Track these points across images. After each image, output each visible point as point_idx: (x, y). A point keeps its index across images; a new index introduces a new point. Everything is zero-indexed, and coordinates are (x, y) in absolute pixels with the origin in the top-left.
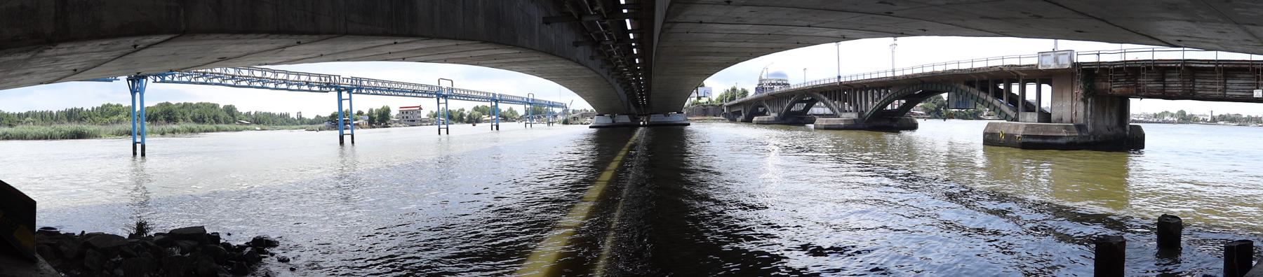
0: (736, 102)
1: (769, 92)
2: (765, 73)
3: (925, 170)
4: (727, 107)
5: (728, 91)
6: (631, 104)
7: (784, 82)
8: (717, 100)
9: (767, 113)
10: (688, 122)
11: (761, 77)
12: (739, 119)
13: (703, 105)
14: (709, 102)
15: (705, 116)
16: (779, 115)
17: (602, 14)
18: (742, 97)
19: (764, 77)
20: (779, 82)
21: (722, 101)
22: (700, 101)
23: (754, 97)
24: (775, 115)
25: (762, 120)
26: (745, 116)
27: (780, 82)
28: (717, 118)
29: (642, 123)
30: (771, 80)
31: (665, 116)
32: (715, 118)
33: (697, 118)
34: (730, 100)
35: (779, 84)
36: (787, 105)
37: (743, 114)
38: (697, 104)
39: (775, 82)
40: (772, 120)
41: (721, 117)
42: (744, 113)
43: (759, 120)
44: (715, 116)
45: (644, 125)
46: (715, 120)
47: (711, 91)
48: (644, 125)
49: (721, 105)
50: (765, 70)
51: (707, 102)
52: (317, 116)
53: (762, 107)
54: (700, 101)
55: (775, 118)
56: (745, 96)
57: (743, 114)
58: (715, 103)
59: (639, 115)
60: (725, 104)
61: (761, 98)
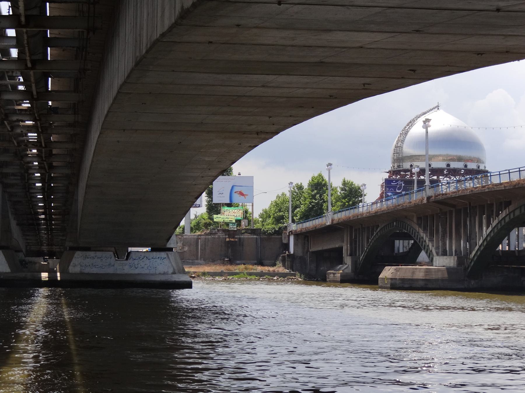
0: (327, 220)
1: (430, 192)
2: (417, 130)
3: (514, 356)
4: (298, 235)
5: (300, 188)
6: (11, 217)
7: (472, 166)
8: (266, 215)
9: (423, 256)
10: (184, 278)
11: (398, 149)
12: (337, 273)
13: (225, 226)
14: (244, 223)
15: (231, 262)
16: (461, 260)
17: (32, 93)
18: (344, 208)
19: (407, 150)
20: (454, 165)
21: (279, 220)
22: (217, 218)
23: (375, 208)
24: (450, 261)
25: (408, 276)
26: (355, 263)
27: (459, 165)
28: (266, 269)
29: (45, 275)
30: (431, 158)
31: (117, 255)
32: (259, 269)
33: (207, 269)
34: (306, 216)
35: (454, 172)
36: (486, 231)
37: (348, 260)
38: (207, 225)
39: (442, 165)
40: (439, 276)
41: (280, 268)
42: (352, 254)
43: (399, 276)
44: (261, 263)
45: (51, 283)
46: (261, 275)
47: (251, 188)
48: (51, 283)
49: (279, 232)
50: (420, 123)
51: (238, 222)
52: (192, 288)
53: (406, 236)
54: (217, 218)
55: (449, 270)
56: (355, 205)
57: (348, 260)
58: (258, 226)
59: (32, 253)
60: (294, 227)
61: (405, 210)
